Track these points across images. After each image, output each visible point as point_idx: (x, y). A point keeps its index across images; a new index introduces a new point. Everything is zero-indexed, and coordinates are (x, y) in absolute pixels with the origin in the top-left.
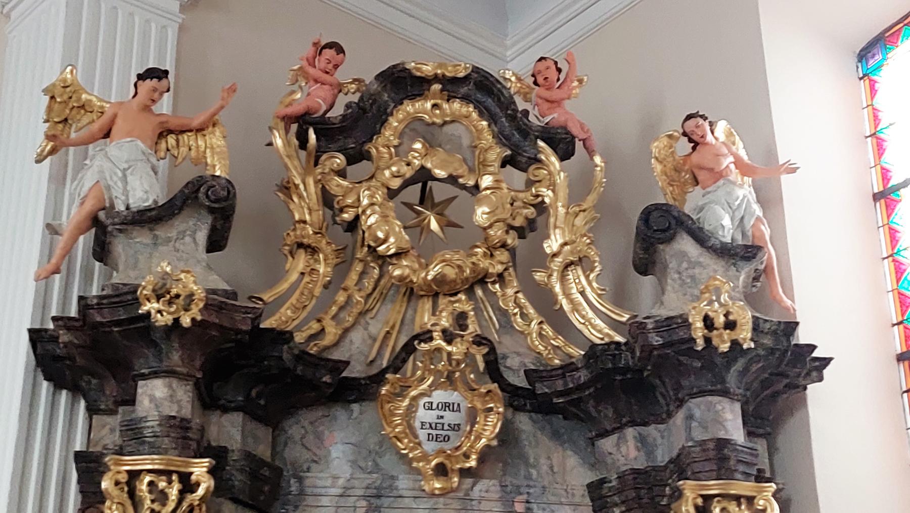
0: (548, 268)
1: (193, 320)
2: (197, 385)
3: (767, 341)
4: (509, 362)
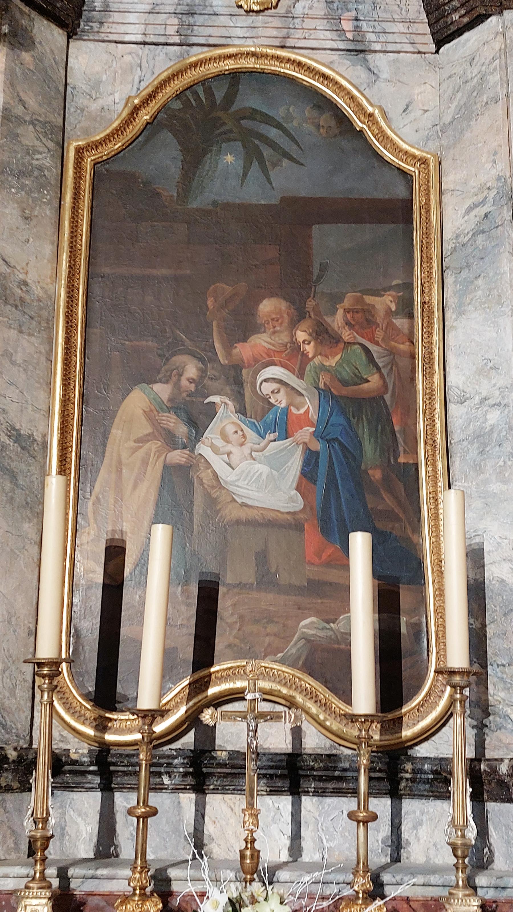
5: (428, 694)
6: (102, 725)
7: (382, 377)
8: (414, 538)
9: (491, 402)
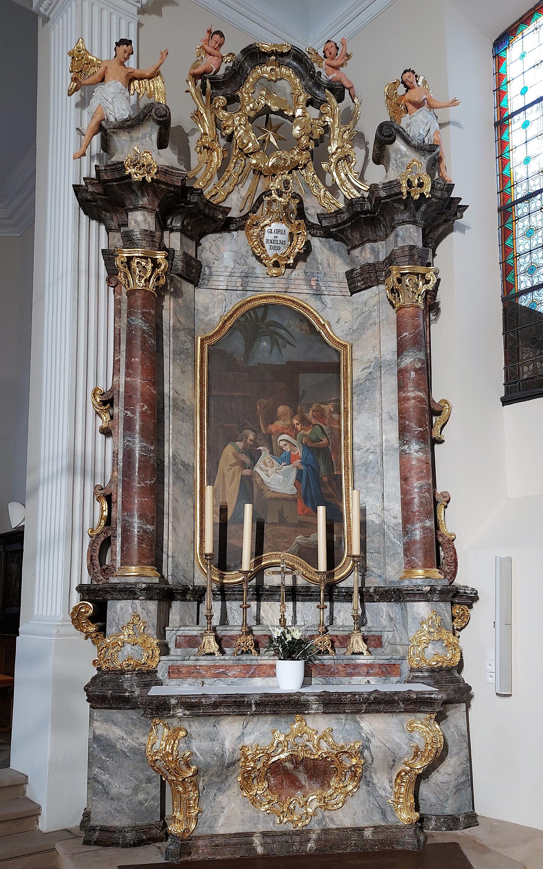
0: (329, 161)
1: (152, 178)
2: (157, 215)
3: (438, 194)
4: (309, 212)
5: (344, 564)
6: (222, 577)
7: (328, 438)
8: (340, 504)
9: (370, 451)
